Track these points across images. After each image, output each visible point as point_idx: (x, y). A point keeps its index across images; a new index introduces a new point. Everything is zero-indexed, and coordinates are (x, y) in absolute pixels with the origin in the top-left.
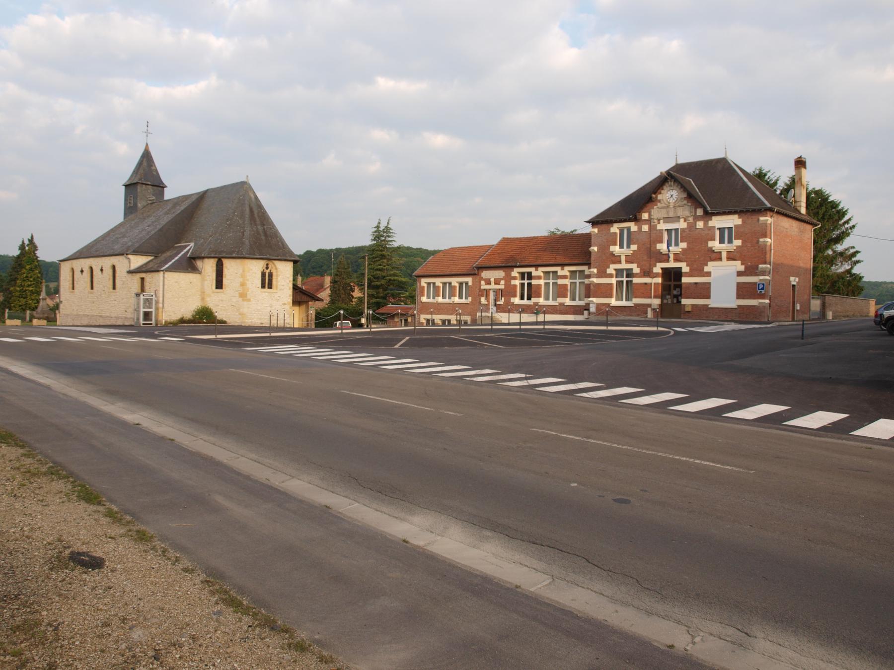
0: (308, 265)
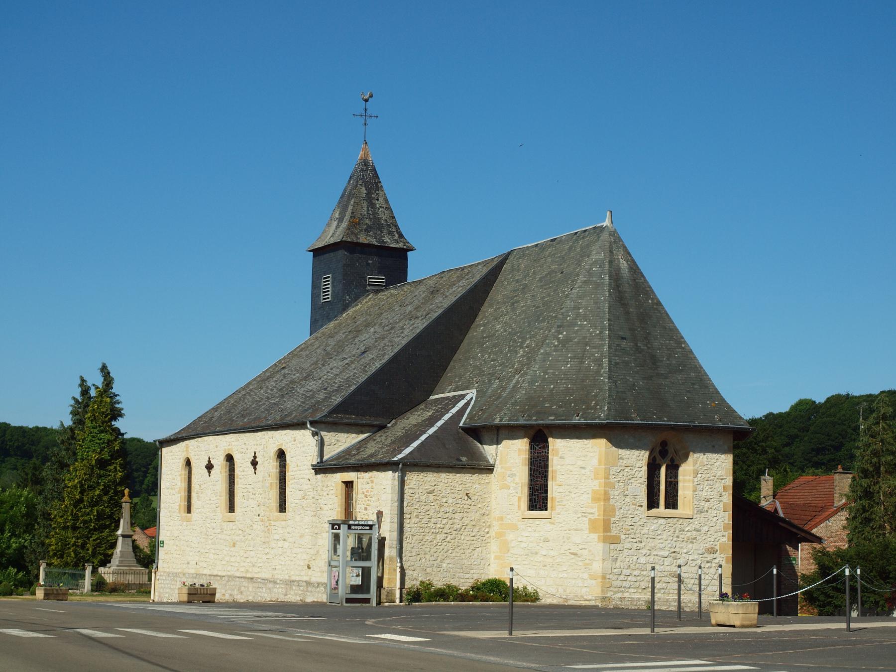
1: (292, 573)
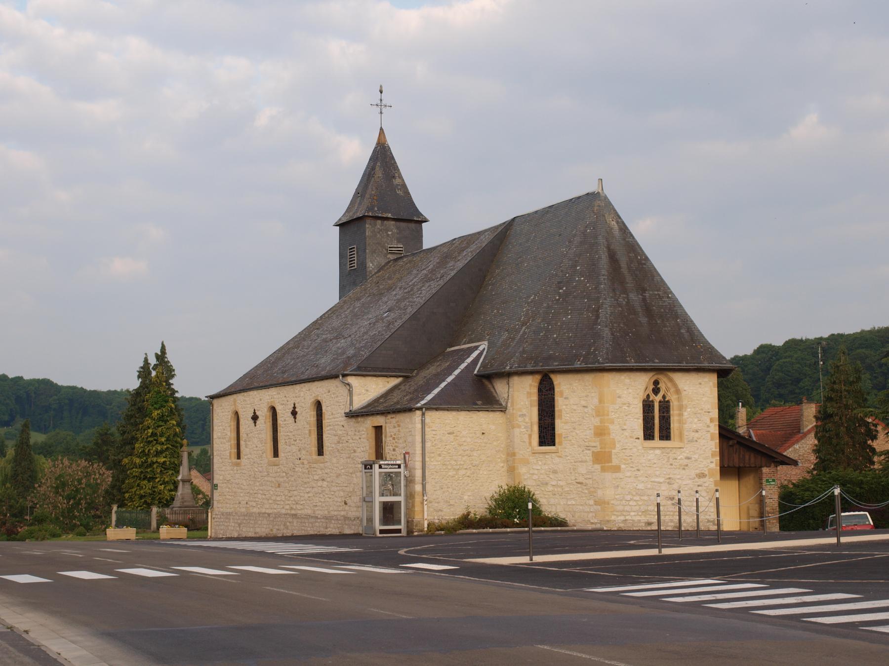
0: (757, 383)
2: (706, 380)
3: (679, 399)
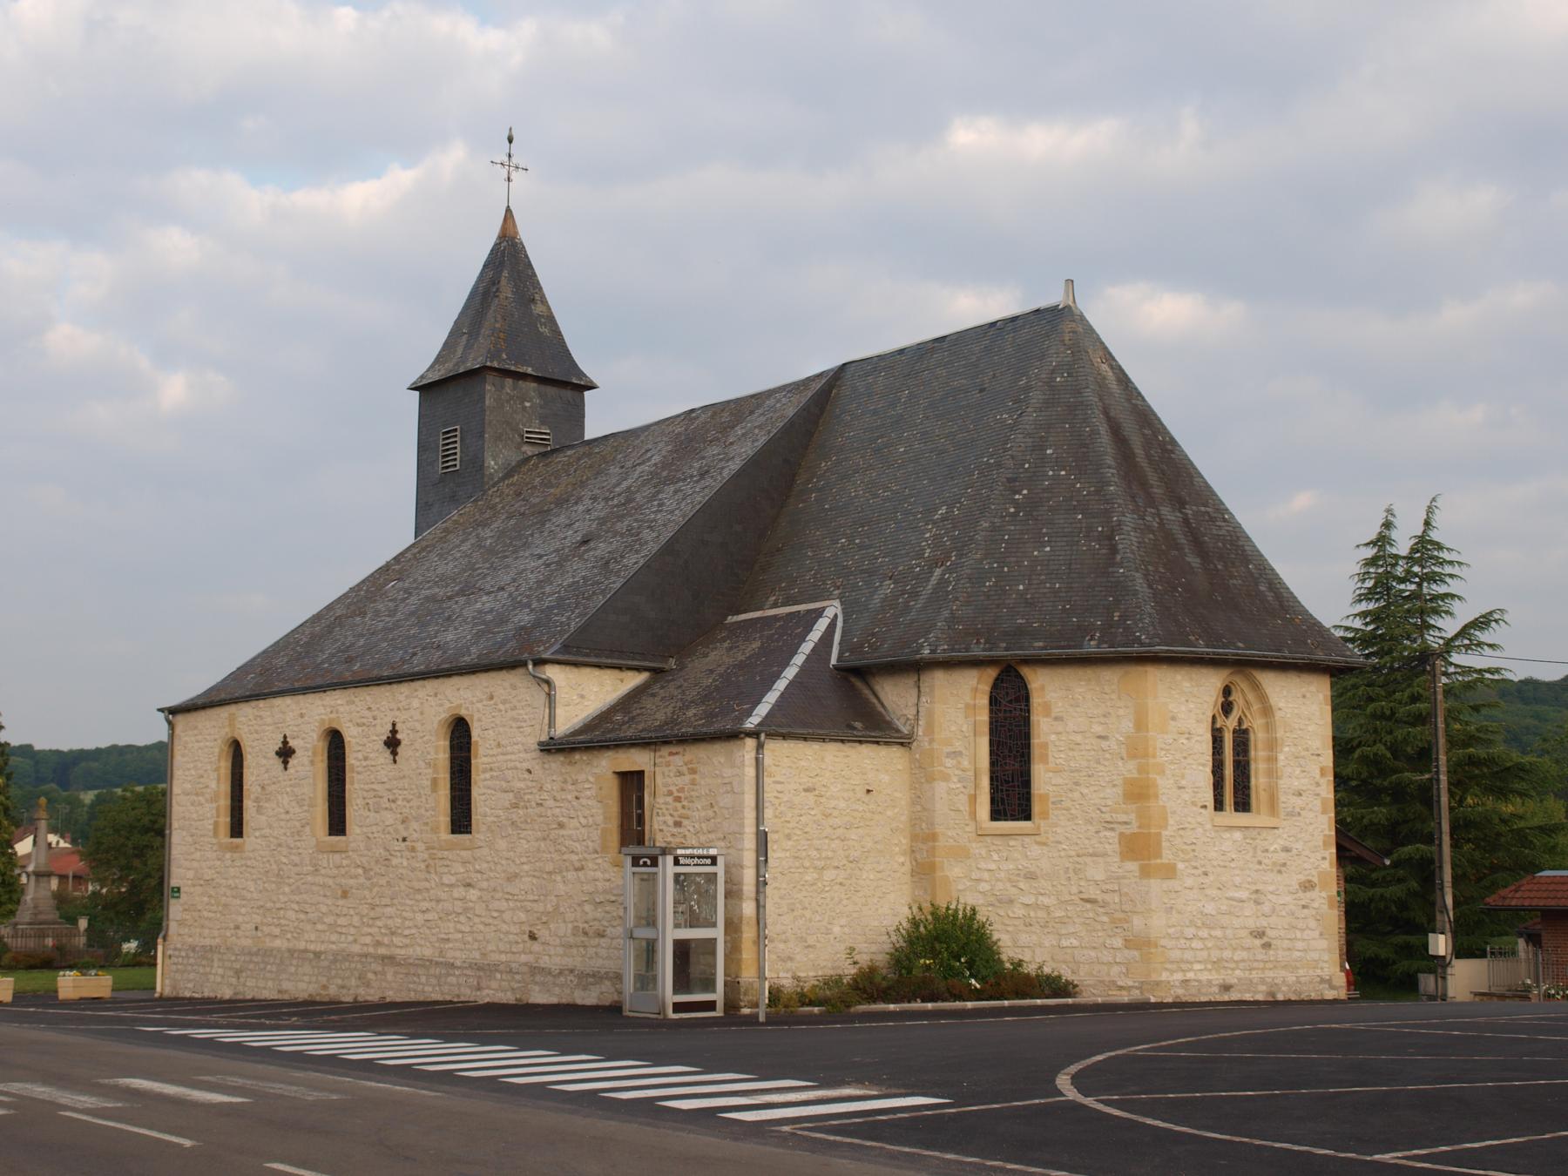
1: (490, 947)
2: (1313, 688)
3: (1269, 727)
